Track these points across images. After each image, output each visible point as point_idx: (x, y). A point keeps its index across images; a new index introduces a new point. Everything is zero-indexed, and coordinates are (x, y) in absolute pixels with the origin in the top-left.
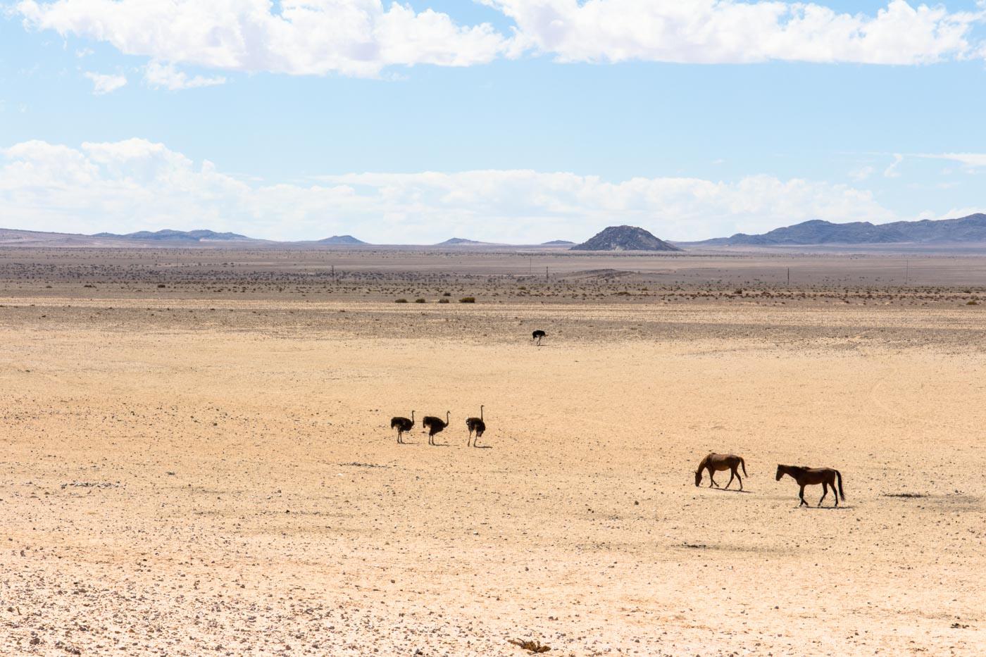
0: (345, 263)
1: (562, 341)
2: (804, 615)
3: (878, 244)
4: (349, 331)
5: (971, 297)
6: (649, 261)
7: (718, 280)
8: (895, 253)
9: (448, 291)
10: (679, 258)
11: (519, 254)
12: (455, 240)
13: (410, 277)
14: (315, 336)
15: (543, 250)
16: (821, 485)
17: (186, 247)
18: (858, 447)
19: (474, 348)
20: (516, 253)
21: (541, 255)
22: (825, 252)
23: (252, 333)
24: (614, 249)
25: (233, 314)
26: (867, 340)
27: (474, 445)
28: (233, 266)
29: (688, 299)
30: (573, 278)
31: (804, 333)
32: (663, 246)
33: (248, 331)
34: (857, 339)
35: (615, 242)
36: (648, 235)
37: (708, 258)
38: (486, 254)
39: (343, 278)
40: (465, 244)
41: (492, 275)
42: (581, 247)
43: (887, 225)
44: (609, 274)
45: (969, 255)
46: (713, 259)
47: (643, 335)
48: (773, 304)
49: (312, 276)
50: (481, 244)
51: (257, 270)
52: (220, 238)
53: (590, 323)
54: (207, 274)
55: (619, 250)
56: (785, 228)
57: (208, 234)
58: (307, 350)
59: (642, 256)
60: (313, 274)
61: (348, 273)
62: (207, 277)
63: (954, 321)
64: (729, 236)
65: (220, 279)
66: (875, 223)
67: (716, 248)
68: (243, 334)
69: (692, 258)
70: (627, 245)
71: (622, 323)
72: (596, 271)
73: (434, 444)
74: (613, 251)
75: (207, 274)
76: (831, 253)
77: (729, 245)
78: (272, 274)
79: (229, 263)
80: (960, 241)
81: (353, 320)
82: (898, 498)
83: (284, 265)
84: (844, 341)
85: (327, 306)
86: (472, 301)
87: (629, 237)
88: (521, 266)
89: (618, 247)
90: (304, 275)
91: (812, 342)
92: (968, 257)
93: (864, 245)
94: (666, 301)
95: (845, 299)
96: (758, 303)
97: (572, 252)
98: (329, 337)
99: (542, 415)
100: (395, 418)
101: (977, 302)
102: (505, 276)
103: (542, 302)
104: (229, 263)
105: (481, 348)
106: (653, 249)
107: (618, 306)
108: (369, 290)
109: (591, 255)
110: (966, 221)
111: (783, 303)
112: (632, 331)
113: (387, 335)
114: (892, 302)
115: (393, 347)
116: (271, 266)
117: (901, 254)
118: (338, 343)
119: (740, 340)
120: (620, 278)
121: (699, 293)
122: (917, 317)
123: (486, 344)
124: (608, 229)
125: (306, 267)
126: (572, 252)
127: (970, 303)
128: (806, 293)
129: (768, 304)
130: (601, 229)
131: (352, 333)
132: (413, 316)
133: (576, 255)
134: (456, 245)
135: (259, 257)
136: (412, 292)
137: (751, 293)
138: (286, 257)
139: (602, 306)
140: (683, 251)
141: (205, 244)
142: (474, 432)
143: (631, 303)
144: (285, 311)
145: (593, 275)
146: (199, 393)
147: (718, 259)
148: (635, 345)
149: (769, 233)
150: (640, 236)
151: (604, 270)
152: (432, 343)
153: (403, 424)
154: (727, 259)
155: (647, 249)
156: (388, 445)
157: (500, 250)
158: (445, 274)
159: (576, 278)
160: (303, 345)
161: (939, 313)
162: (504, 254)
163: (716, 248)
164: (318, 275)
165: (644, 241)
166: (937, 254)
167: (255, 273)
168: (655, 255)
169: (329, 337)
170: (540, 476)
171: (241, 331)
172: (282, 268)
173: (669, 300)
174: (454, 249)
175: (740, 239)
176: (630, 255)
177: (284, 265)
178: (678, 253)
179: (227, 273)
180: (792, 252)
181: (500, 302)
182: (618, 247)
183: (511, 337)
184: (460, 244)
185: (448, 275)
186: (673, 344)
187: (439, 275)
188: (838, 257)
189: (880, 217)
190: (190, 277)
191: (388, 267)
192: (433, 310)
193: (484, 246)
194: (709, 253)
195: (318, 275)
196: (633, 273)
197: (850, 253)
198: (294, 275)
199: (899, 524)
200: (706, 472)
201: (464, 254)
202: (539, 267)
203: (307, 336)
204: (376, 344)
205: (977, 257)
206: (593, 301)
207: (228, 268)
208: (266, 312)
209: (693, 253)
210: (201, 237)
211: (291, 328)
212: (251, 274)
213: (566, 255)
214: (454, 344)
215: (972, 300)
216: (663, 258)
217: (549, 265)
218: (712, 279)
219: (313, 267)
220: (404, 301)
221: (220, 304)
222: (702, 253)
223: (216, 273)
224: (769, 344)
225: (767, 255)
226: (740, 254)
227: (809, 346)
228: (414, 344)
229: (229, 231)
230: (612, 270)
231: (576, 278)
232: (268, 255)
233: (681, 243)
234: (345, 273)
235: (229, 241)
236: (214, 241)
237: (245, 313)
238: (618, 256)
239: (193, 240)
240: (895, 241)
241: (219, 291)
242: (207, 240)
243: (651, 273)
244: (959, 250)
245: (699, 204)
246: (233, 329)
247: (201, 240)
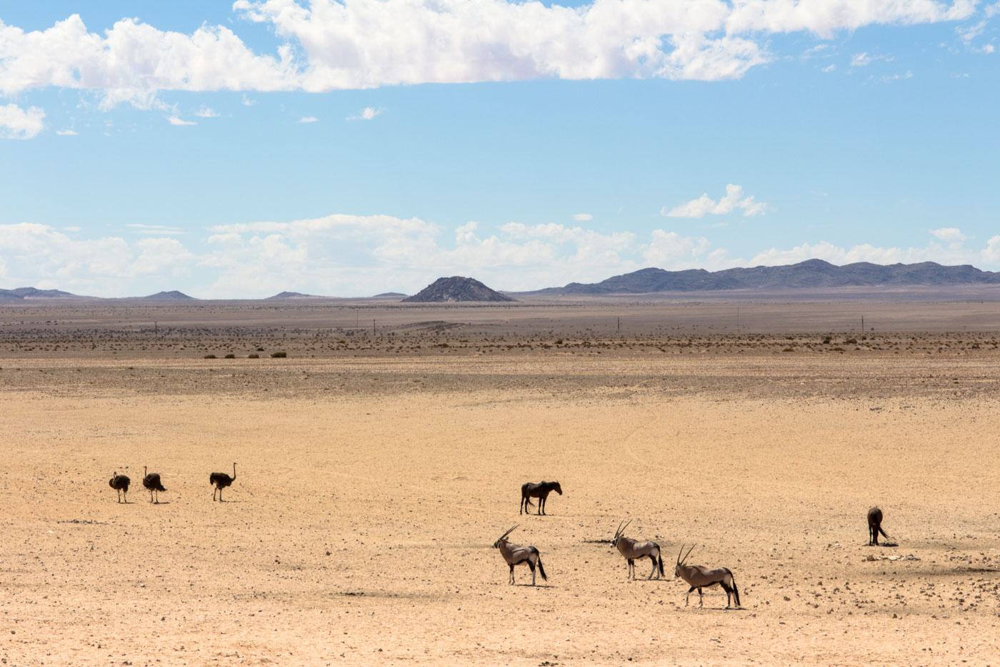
0: (172, 319)
1: (341, 394)
2: (401, 657)
3: (714, 291)
4: (131, 388)
5: (973, 341)
6: (481, 312)
7: (550, 330)
8: (730, 301)
10: (512, 309)
11: (350, 307)
12: (285, 294)
13: (237, 333)
14: (95, 394)
15: (374, 303)
17: (10, 306)
18: (589, 495)
19: (251, 404)
20: (346, 306)
21: (372, 307)
22: (661, 300)
23: (31, 392)
24: (447, 300)
25: (19, 373)
26: (644, 389)
27: (221, 500)
28: (56, 324)
29: (503, 350)
30: (402, 330)
31: (581, 383)
32: (496, 296)
33: (28, 390)
34: (635, 388)
35: (447, 292)
36: (481, 286)
37: (541, 309)
38: (316, 307)
39: (168, 334)
40: (295, 298)
41: (321, 329)
43: (723, 272)
44: (440, 326)
45: (797, 301)
46: (546, 309)
47: (424, 387)
48: (589, 353)
49: (136, 332)
50: (312, 298)
51: (80, 327)
52: (46, 295)
53: (375, 377)
54: (29, 333)
55: (451, 302)
56: (619, 277)
57: (33, 292)
58: (82, 409)
59: (474, 307)
60: (138, 330)
61: (174, 329)
62: (29, 336)
63: (758, 368)
64: (563, 286)
65: (42, 338)
66: (710, 271)
67: (551, 298)
68: (22, 393)
69: (524, 309)
70: (459, 296)
71: (407, 376)
72: (427, 323)
74: (445, 303)
75: (29, 333)
76: (666, 301)
77: (563, 295)
78: (96, 331)
79: (53, 321)
80: (797, 287)
81: (139, 376)
82: (596, 544)
83: (109, 322)
84: (622, 390)
85: (133, 363)
86: (284, 356)
87: (461, 288)
88: (349, 319)
89: (450, 299)
90: (129, 332)
91: (590, 391)
92: (804, 303)
93: (698, 293)
94: (481, 353)
95: (662, 348)
96: (573, 353)
97: (403, 304)
98: (109, 394)
99: (291, 470)
100: (213, 474)
101: (794, 348)
102: (333, 329)
103: (355, 356)
104: (53, 321)
105: (258, 403)
106: (485, 300)
107: (434, 359)
108: (185, 346)
109: (423, 306)
110: (802, 267)
111: (599, 353)
112: (415, 384)
113: (168, 392)
114: (708, 350)
115: (170, 403)
116: (95, 323)
117: (736, 301)
118: (115, 400)
119: (519, 390)
120: (452, 330)
121: (519, 344)
122: (720, 365)
123: (266, 399)
124: (440, 280)
125: (132, 324)
126: (403, 304)
127: (786, 350)
128: (628, 343)
129: (583, 354)
131: (133, 390)
132: (201, 372)
133: (407, 307)
134: (286, 298)
135: (83, 315)
136: (228, 347)
138: (111, 315)
139: (416, 359)
140: (517, 301)
141: (28, 301)
142: (122, 491)
143: (446, 355)
144: (72, 369)
145: (421, 327)
147: (551, 309)
148: (413, 398)
149: (604, 281)
150: (472, 287)
151: (434, 322)
152: (210, 399)
153: (121, 483)
154: (561, 309)
155: (480, 300)
156: (108, 504)
157: (331, 303)
158: (273, 328)
159: (406, 330)
160: (79, 403)
161: (748, 361)
162: (335, 307)
163: (551, 298)
164: (143, 332)
165: (476, 292)
166: (773, 301)
167: (78, 330)
168: (488, 306)
169: (109, 394)
170: (252, 529)
171: (21, 390)
172: (107, 325)
173: (484, 352)
174: (285, 302)
175: (574, 288)
176: (461, 307)
177: (109, 322)
178: (511, 303)
179: (50, 331)
180: (627, 301)
181: (313, 356)
182: (450, 299)
183: (291, 392)
184: (290, 298)
185: (276, 330)
186: (451, 396)
187: (267, 329)
188: (672, 305)
189: (715, 263)
190: (11, 336)
191: (216, 323)
192: (241, 366)
194: (542, 303)
195: (143, 332)
196: (464, 324)
197: (686, 301)
198: (119, 332)
199: (576, 570)
201: (293, 308)
202: (366, 320)
203: (87, 394)
204: (154, 401)
205: (813, 303)
206: (407, 354)
207: (51, 327)
208: (53, 371)
209: (526, 304)
210: (25, 296)
211: (73, 386)
212: (75, 332)
213: (397, 307)
214: (233, 399)
215: (789, 347)
216: (495, 309)
217: (377, 317)
218: (545, 329)
219: (138, 324)
220: (213, 357)
221: (29, 363)
222: (536, 303)
223: (38, 332)
224: (547, 394)
225: (602, 305)
226: (574, 303)
227: (585, 396)
228: (192, 400)
229: (54, 289)
230: (442, 322)
231: (406, 330)
232: (92, 312)
233: (515, 293)
234: (170, 330)
235: (54, 298)
236: (39, 298)
237: (31, 372)
238: (449, 307)
239: (17, 299)
240: (730, 288)
241: (30, 350)
242: (31, 298)
243: (483, 325)
244: (795, 297)
245: (534, 252)
246: (13, 388)
247: (26, 298)
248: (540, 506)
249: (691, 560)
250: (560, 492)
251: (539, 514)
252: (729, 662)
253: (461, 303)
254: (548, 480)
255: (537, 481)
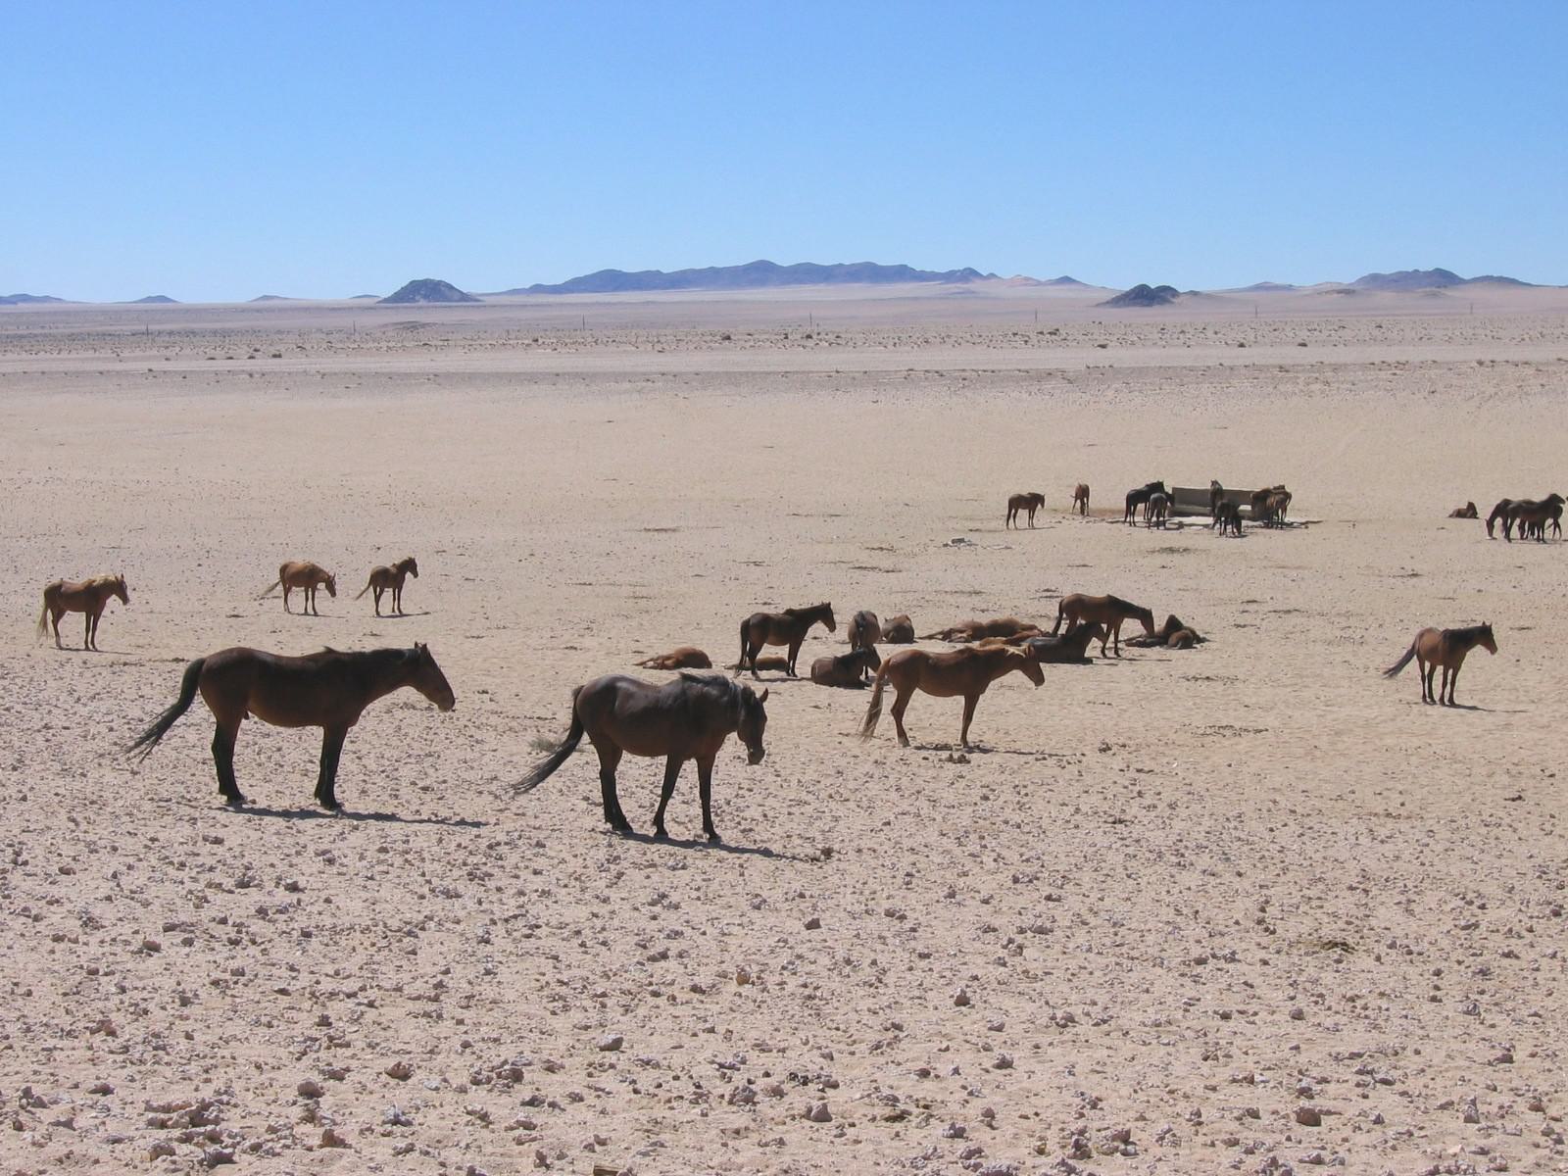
9: (258, 347)
16: (961, 699)
32: (465, 297)
36: (451, 288)
42: (386, 300)
55: (422, 303)
64: (527, 287)
66: (665, 272)
72: (401, 324)
73: (97, 651)
86: (280, 356)
124: (411, 283)
130: (405, 284)
137: (547, 341)
146: (1269, 375)
193: (67, 313)
200: (1499, 521)
248: (307, 599)
249: (732, 742)
250: (125, 600)
251: (306, 613)
252: (728, 1173)
253: (431, 304)
254: (99, 577)
255: (77, 580)
